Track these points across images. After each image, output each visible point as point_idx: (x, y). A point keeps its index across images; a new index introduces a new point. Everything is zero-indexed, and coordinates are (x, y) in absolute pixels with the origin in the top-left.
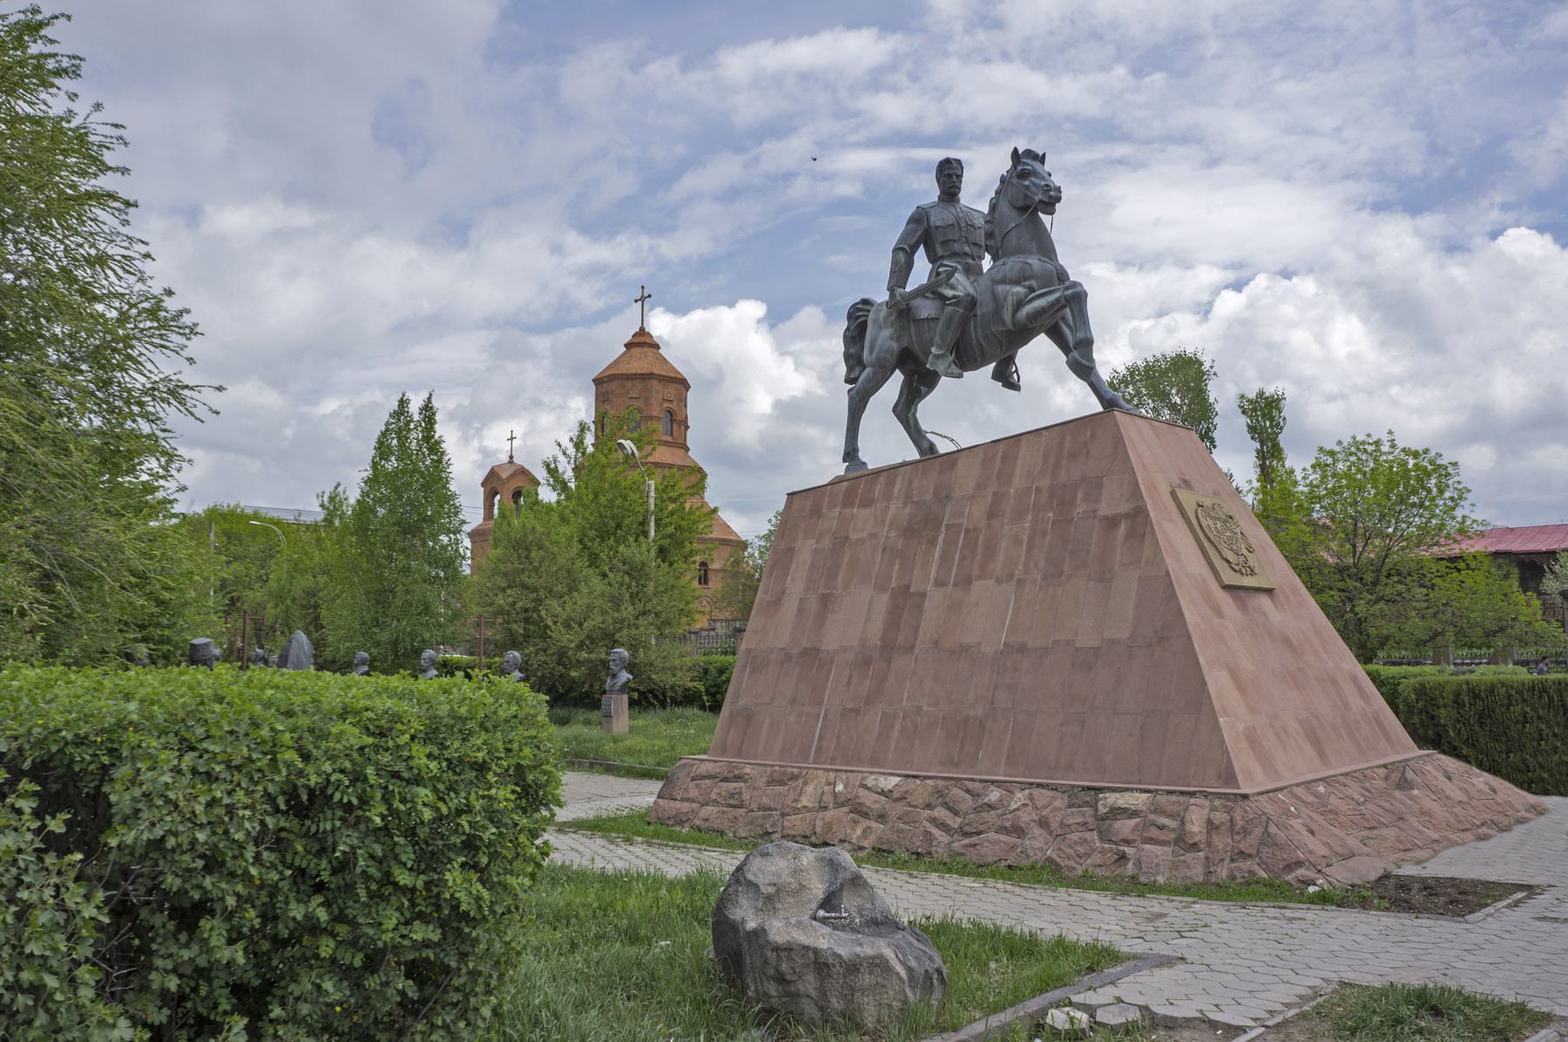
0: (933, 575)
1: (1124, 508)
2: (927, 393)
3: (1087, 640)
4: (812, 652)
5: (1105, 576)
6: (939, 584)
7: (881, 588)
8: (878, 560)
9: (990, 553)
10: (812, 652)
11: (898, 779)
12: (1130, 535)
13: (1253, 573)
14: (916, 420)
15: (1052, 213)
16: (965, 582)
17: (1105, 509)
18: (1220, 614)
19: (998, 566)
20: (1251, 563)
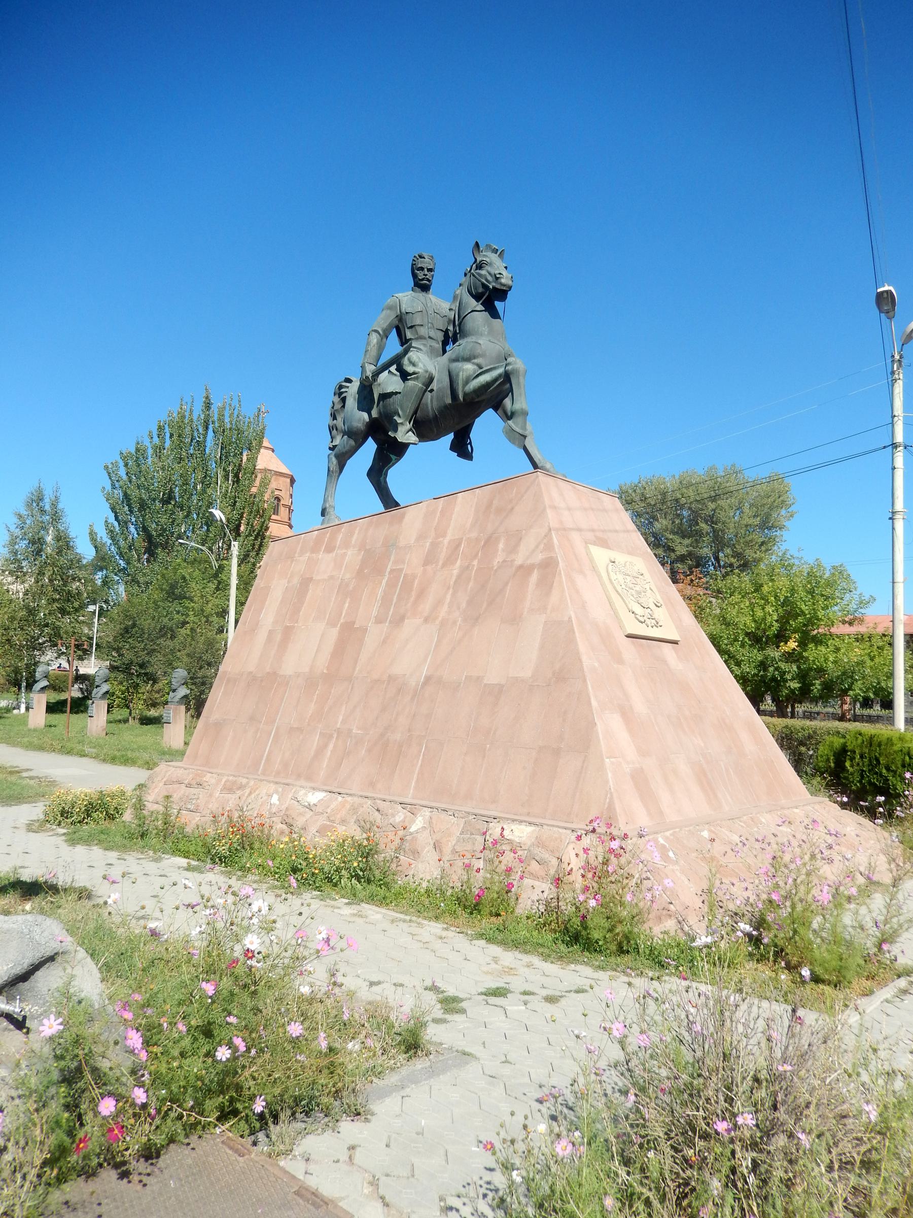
0: (375, 613)
1: (539, 557)
2: (397, 461)
3: (493, 677)
4: (273, 676)
5: (515, 619)
6: (379, 621)
7: (332, 624)
10: (273, 676)
11: (324, 794)
13: (657, 625)
14: (386, 482)
16: (399, 620)
17: (519, 560)
18: (620, 661)
19: (426, 607)
20: (655, 616)
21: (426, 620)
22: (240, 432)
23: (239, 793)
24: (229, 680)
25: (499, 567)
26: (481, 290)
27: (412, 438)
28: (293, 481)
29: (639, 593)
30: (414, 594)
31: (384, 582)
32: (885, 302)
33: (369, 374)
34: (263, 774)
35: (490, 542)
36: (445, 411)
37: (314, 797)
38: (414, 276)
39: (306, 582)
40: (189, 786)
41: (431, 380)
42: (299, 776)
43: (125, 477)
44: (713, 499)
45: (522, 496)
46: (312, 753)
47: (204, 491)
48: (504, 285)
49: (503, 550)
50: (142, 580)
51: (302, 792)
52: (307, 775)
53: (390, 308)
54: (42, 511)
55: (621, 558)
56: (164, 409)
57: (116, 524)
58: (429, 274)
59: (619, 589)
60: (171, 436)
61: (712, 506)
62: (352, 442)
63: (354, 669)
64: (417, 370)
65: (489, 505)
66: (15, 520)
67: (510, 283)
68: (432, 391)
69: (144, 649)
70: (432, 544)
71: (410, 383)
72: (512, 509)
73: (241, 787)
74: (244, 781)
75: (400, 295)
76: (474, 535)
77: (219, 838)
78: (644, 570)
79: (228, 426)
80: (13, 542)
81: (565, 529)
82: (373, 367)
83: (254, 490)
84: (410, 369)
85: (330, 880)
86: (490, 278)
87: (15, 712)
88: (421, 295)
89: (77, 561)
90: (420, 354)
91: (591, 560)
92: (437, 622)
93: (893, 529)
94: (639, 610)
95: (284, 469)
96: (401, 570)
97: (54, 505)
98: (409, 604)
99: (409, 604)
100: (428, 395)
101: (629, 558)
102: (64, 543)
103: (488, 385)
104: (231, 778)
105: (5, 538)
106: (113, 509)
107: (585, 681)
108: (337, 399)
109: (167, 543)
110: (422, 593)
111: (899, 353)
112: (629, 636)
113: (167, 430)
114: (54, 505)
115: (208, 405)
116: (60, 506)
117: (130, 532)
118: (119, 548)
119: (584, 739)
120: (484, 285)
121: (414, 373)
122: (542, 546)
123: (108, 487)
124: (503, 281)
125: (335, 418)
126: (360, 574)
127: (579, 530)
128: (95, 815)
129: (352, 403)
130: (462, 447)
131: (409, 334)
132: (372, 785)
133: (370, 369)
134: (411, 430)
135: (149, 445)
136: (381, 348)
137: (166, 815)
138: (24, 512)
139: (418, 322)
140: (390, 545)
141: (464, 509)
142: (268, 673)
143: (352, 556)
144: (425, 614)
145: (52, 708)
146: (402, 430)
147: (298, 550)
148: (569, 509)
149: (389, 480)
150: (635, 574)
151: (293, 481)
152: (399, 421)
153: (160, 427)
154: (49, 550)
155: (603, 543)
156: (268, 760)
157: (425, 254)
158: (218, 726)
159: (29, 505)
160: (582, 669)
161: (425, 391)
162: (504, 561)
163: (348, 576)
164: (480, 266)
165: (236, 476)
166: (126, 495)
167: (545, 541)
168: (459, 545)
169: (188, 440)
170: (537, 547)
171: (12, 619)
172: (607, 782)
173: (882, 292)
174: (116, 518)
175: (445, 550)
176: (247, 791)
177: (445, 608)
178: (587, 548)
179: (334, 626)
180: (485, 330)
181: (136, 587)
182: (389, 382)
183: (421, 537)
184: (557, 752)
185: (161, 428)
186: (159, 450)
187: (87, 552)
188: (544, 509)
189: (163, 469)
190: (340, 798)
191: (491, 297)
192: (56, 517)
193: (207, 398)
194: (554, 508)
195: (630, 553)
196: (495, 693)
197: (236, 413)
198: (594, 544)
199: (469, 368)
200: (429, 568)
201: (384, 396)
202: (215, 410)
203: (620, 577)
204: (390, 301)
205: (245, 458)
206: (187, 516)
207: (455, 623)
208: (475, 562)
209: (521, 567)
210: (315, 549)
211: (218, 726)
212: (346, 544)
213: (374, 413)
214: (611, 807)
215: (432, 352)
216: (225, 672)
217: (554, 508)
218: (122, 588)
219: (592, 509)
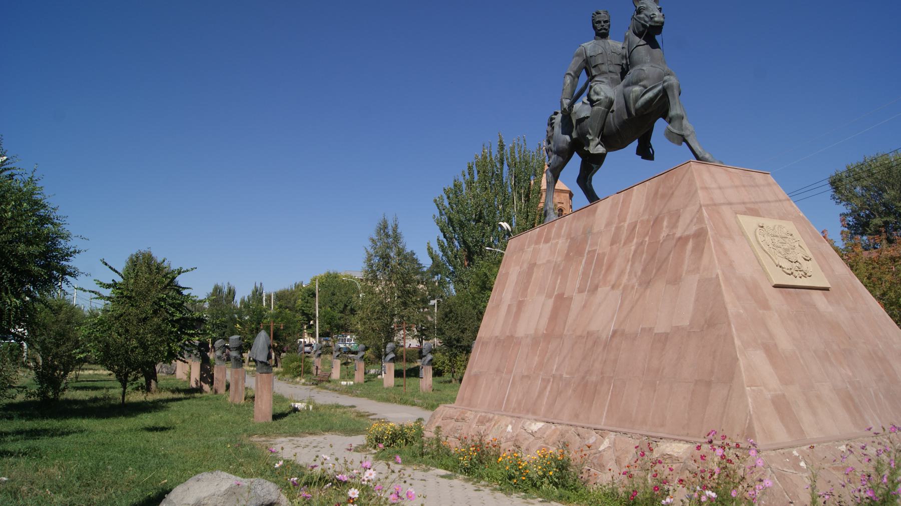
0: (577, 286)
1: (694, 229)
3: (661, 328)
4: (511, 337)
5: (676, 280)
6: (581, 291)
7: (549, 296)
10: (511, 337)
14: (591, 186)
17: (679, 233)
18: (765, 306)
19: (613, 277)
21: (613, 287)
22: (527, 163)
23: (488, 424)
24: (483, 343)
25: (664, 241)
26: (641, 29)
27: (601, 149)
28: (571, 195)
29: (787, 250)
30: (604, 268)
33: (566, 106)
34: (505, 410)
35: (657, 221)
36: (624, 124)
37: (536, 426)
38: (595, 28)
39: (532, 266)
40: (457, 420)
41: (611, 103)
42: (528, 412)
43: (448, 206)
46: (536, 394)
47: (504, 210)
48: (657, 22)
49: (667, 227)
50: (465, 279)
51: (529, 422)
52: (532, 411)
53: (578, 55)
54: (388, 236)
55: (769, 223)
56: (471, 154)
57: (445, 240)
58: (606, 25)
59: (766, 248)
60: (479, 172)
62: (560, 159)
64: (599, 97)
65: (656, 193)
66: (370, 243)
67: (662, 19)
69: (458, 329)
71: (596, 108)
72: (672, 194)
73: (489, 420)
74: (491, 416)
75: (585, 44)
76: (646, 217)
77: (462, 454)
78: (795, 233)
79: (518, 160)
80: (369, 259)
81: (715, 205)
82: (568, 101)
83: (541, 205)
84: (595, 98)
85: (534, 485)
86: (647, 19)
87: (379, 377)
88: (601, 42)
89: (418, 269)
90: (602, 86)
91: (740, 227)
92: (621, 288)
94: (786, 264)
95: (567, 189)
96: (595, 251)
97: (395, 230)
98: (601, 277)
99: (601, 277)
100: (611, 115)
101: (777, 222)
102: (411, 258)
103: (651, 100)
104: (483, 414)
105: (364, 256)
106: (442, 230)
107: (729, 325)
108: (549, 129)
109: (481, 251)
110: (610, 267)
112: (776, 286)
113: (475, 169)
114: (395, 230)
115: (502, 147)
116: (399, 231)
117: (455, 246)
118: (448, 257)
119: (728, 372)
120: (643, 26)
121: (598, 100)
122: (695, 220)
123: (438, 214)
124: (656, 19)
125: (549, 143)
126: (567, 257)
127: (730, 204)
128: (398, 441)
129: (558, 129)
130: (645, 152)
131: (594, 72)
132: (577, 416)
133: (566, 102)
134: (599, 143)
135: (462, 181)
136: (574, 85)
137: (438, 440)
138: (375, 238)
139: (600, 62)
140: (588, 232)
141: (639, 196)
143: (562, 244)
144: (612, 283)
145: (398, 374)
146: (592, 144)
148: (720, 188)
149: (593, 183)
150: (784, 235)
151: (571, 195)
152: (590, 138)
153: (469, 168)
154: (393, 263)
155: (753, 212)
156: (508, 400)
157: (600, 11)
158: (477, 377)
159: (378, 233)
160: (727, 316)
161: (608, 113)
162: (668, 235)
163: (559, 259)
164: (639, 11)
165: (527, 196)
166: (450, 219)
168: (635, 227)
169: (490, 174)
170: (692, 221)
171: (373, 312)
172: (747, 406)
174: (445, 236)
176: (493, 423)
177: (626, 276)
178: (736, 217)
179: (551, 297)
180: (648, 59)
181: (461, 285)
182: (581, 109)
183: (608, 224)
184: (709, 384)
185: (470, 168)
186: (470, 184)
187: (426, 262)
188: (696, 191)
189: (474, 197)
190: (553, 427)
191: (650, 33)
192: (397, 238)
193: (501, 141)
194: (705, 188)
195: (781, 218)
196: (663, 339)
197: (523, 150)
198: (745, 213)
199: (637, 89)
200: (614, 247)
201: (580, 121)
202: (507, 149)
203: (768, 239)
204: (578, 50)
205: (532, 182)
206: (493, 230)
207: (633, 287)
208: (647, 239)
209: (680, 238)
210: (537, 242)
211: (477, 377)
212: (558, 236)
213: (574, 135)
214: (750, 428)
215: (614, 83)
216: (480, 337)
217: (705, 188)
218: (452, 287)
219: (744, 186)
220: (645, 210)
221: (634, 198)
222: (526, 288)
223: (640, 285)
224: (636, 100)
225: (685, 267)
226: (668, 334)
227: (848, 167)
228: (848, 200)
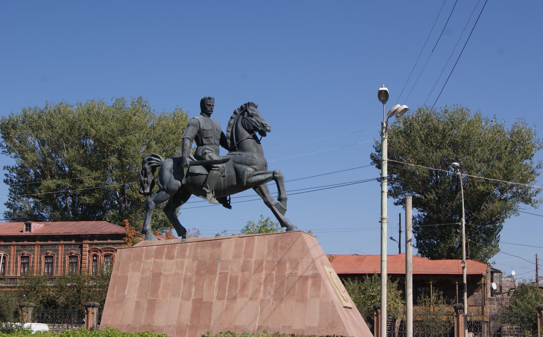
0: (215, 294)
1: (310, 273)
5: (303, 299)
6: (219, 298)
7: (186, 298)
8: (182, 286)
9: (244, 286)
12: (314, 284)
15: (376, 167)
19: (250, 291)
25: (289, 276)
31: (217, 279)
32: (383, 96)
35: (281, 263)
44: (122, 133)
45: (294, 242)
61: (122, 140)
63: (210, 322)
65: (276, 244)
68: (224, 176)
70: (244, 261)
72: (290, 248)
76: (270, 258)
86: (258, 124)
92: (259, 300)
93: (382, 228)
98: (238, 291)
99: (238, 291)
111: (386, 122)
122: (311, 268)
126: (198, 273)
131: (205, 141)
139: (210, 136)
142: (144, 325)
144: (250, 296)
147: (144, 256)
162: (291, 273)
167: (312, 265)
170: (308, 268)
173: (382, 91)
175: (253, 265)
178: (323, 267)
179: (188, 300)
200: (245, 273)
207: (269, 301)
209: (301, 277)
220: (268, 254)
221: (256, 244)
222: (154, 291)
223: (275, 300)
224: (250, 176)
225: (309, 294)
226: (304, 330)
227: (24, 111)
228: (21, 154)
